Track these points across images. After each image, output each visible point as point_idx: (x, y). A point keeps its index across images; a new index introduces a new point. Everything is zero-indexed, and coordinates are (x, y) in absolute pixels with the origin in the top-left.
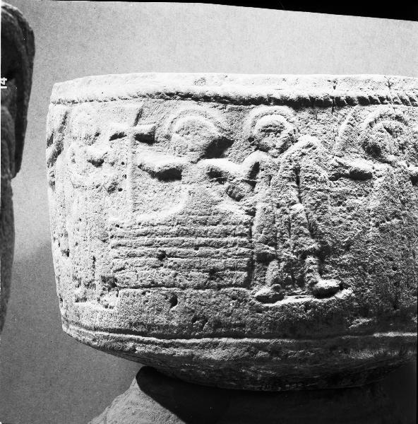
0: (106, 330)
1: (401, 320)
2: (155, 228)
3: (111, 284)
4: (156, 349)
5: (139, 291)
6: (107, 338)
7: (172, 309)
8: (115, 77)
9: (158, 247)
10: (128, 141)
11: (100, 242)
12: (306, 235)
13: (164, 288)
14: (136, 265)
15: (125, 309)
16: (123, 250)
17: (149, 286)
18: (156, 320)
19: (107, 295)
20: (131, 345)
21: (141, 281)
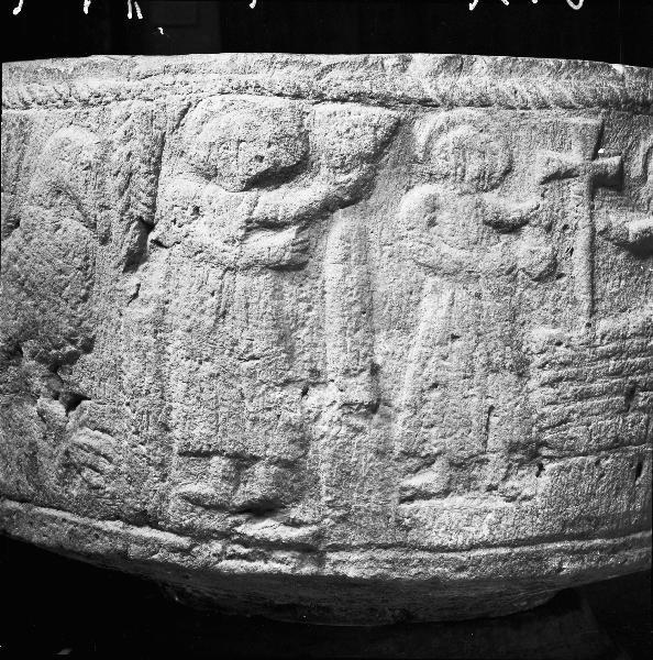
0: (504, 545)
1: (649, 371)
2: (628, 342)
3: (528, 453)
4: (600, 559)
5: (591, 459)
6: (505, 559)
7: (637, 483)
8: (532, 64)
9: (628, 375)
10: (577, 187)
11: (511, 377)
12: (251, 213)
13: (630, 447)
14: (590, 412)
15: (558, 499)
16: (569, 389)
17: (609, 448)
18: (612, 507)
19: (513, 477)
20: (554, 563)
21: (598, 440)
